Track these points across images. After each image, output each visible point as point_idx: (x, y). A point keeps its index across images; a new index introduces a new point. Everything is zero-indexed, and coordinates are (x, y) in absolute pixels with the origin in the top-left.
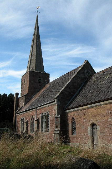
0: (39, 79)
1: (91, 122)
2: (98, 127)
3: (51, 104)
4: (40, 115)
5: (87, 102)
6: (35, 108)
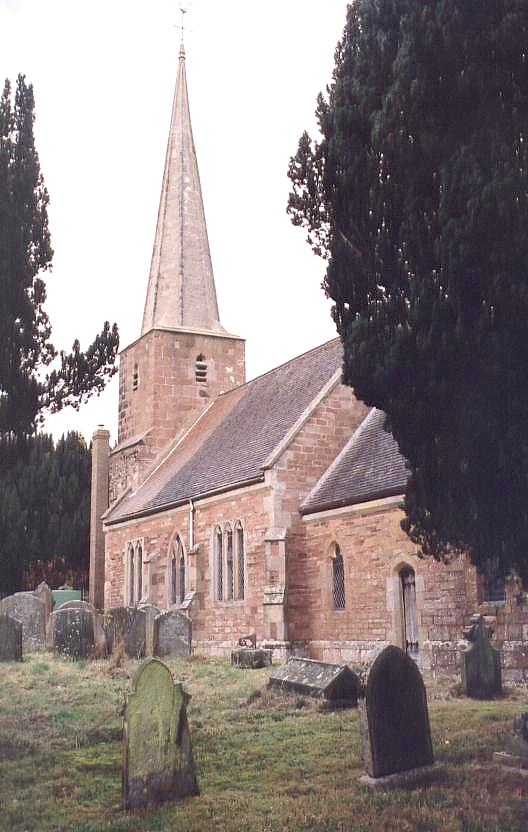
0: (200, 367)
1: (397, 561)
2: (418, 579)
3: (252, 488)
4: (210, 533)
5: (383, 487)
6: (187, 502)
